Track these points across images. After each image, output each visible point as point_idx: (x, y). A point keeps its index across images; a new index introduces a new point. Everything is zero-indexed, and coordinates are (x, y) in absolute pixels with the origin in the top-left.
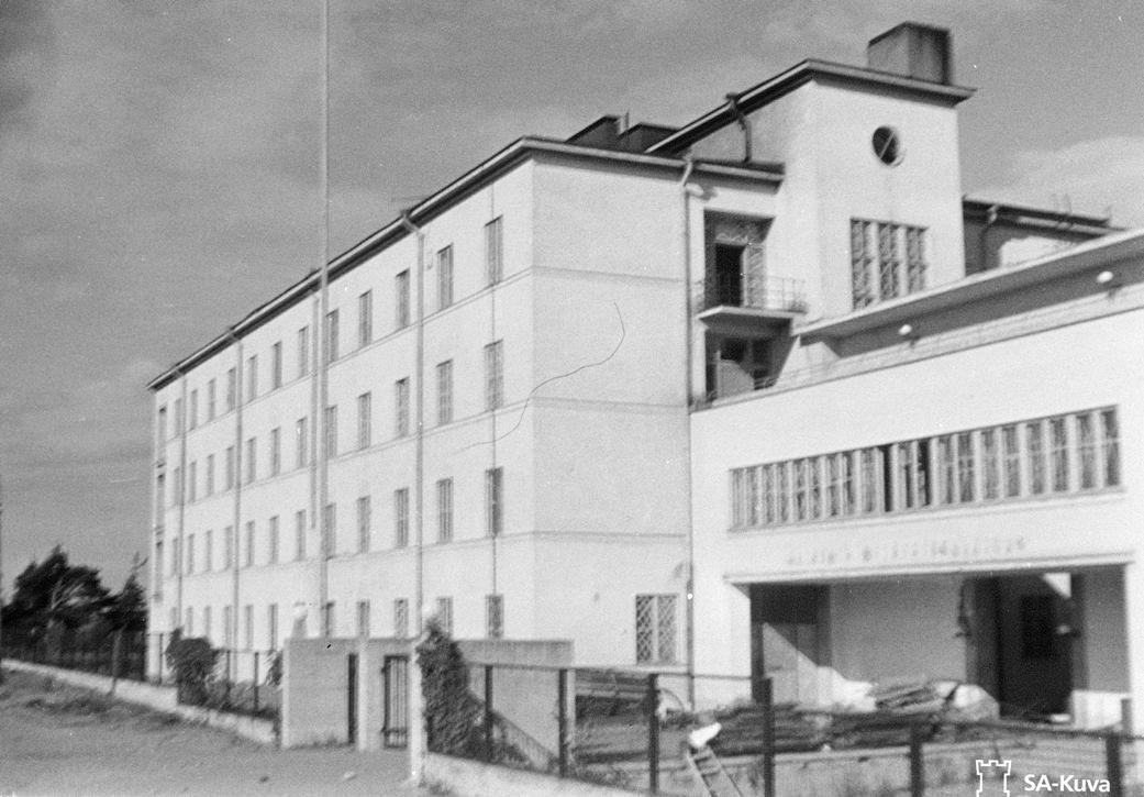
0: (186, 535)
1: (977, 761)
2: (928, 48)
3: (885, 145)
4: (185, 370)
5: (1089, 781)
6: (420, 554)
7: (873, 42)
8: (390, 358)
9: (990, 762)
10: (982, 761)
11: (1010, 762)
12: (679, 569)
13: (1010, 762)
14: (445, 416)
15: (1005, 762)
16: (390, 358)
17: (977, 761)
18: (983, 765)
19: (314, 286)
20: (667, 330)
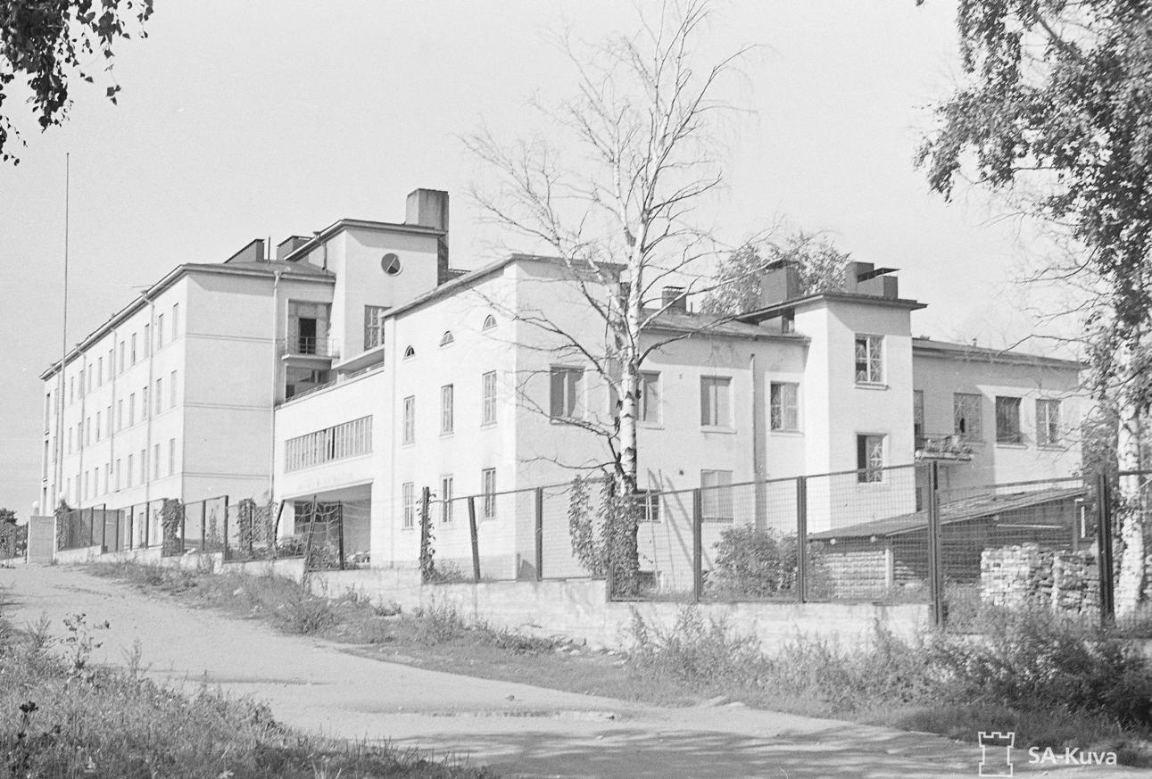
0: (84, 472)
1: (980, 733)
2: (433, 204)
3: (391, 266)
4: (153, 296)
5: (1095, 754)
6: (148, 485)
7: (409, 196)
8: (136, 378)
9: (993, 733)
10: (984, 733)
11: (1013, 734)
12: (267, 493)
13: (1013, 734)
14: (158, 412)
15: (1009, 733)
16: (136, 378)
17: (980, 733)
18: (985, 737)
19: (59, 368)
20: (263, 366)
